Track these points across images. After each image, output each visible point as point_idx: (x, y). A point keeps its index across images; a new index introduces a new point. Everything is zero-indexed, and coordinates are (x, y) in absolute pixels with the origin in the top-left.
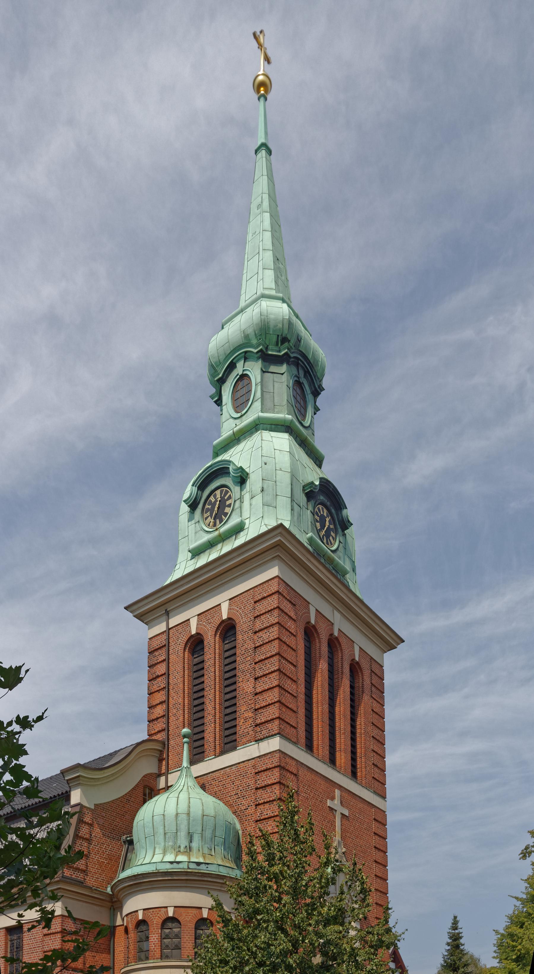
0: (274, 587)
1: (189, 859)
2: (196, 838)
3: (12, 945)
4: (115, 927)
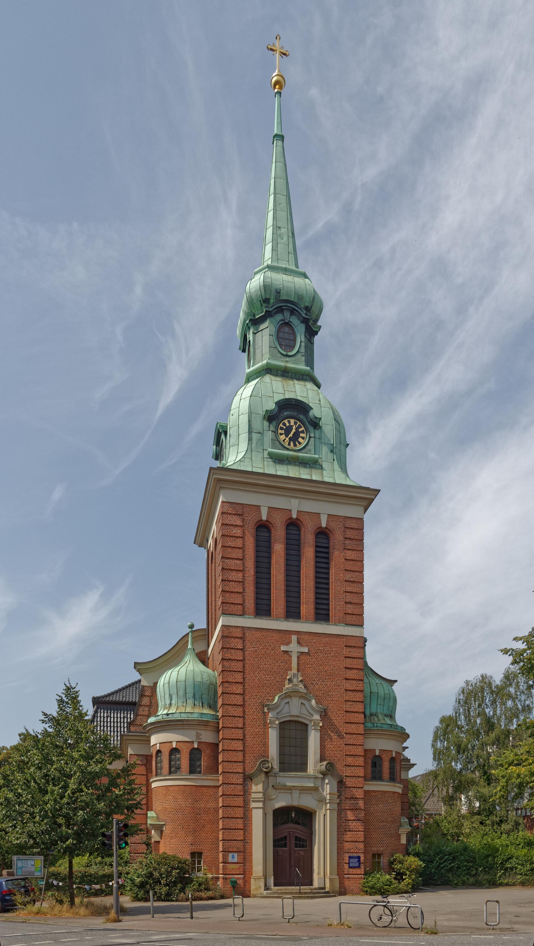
2: (174, 697)
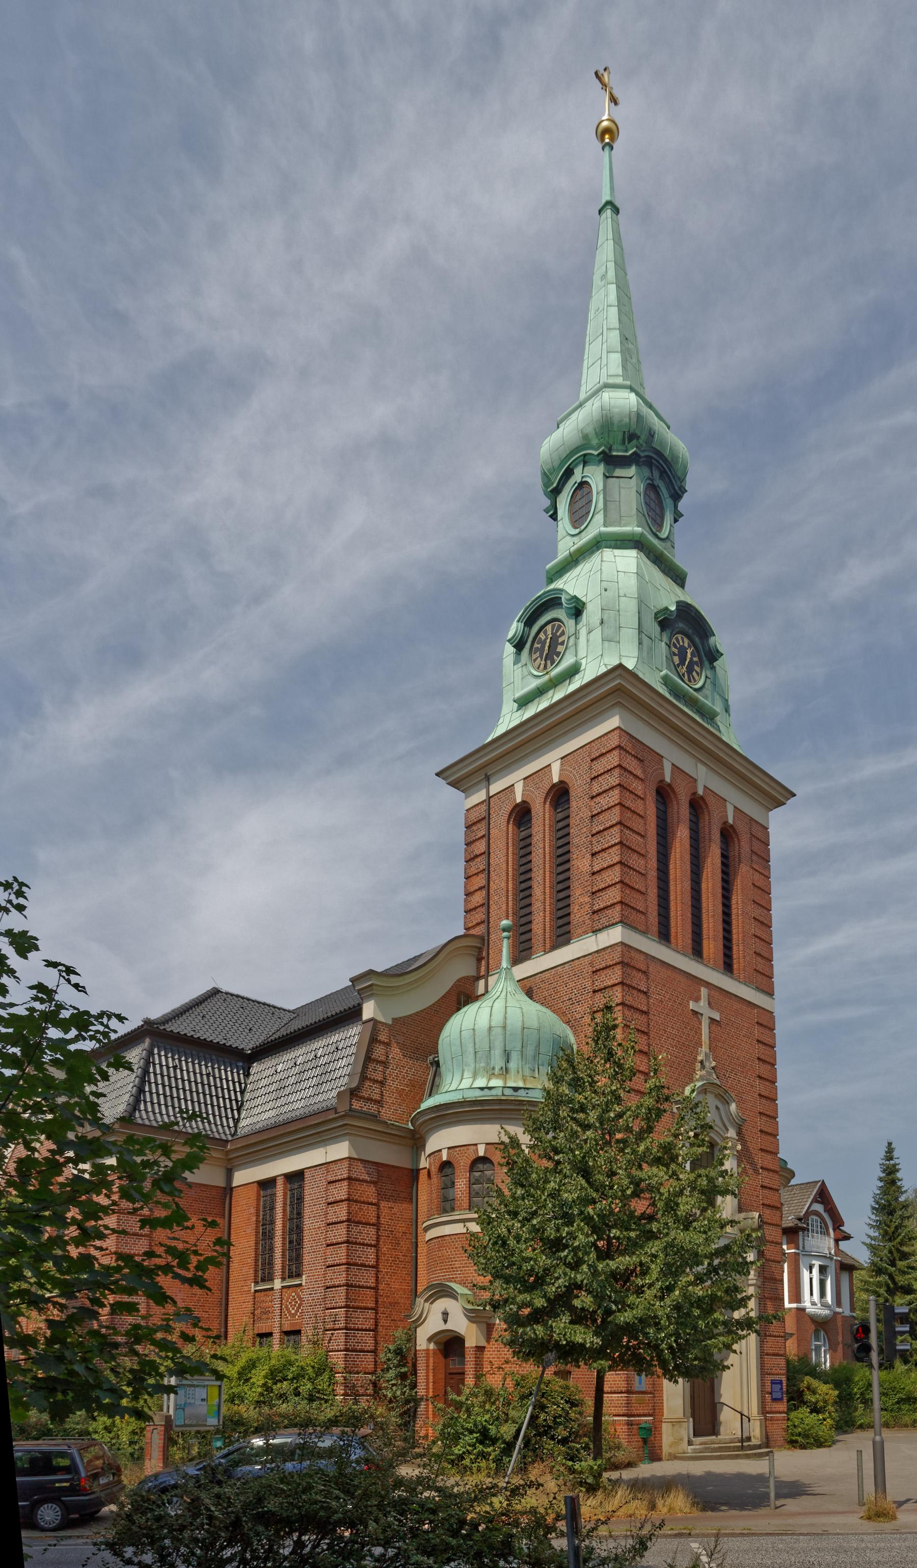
0: (614, 741)
1: (505, 1083)
2: (515, 1056)
3: (292, 1196)
4: (418, 1170)
